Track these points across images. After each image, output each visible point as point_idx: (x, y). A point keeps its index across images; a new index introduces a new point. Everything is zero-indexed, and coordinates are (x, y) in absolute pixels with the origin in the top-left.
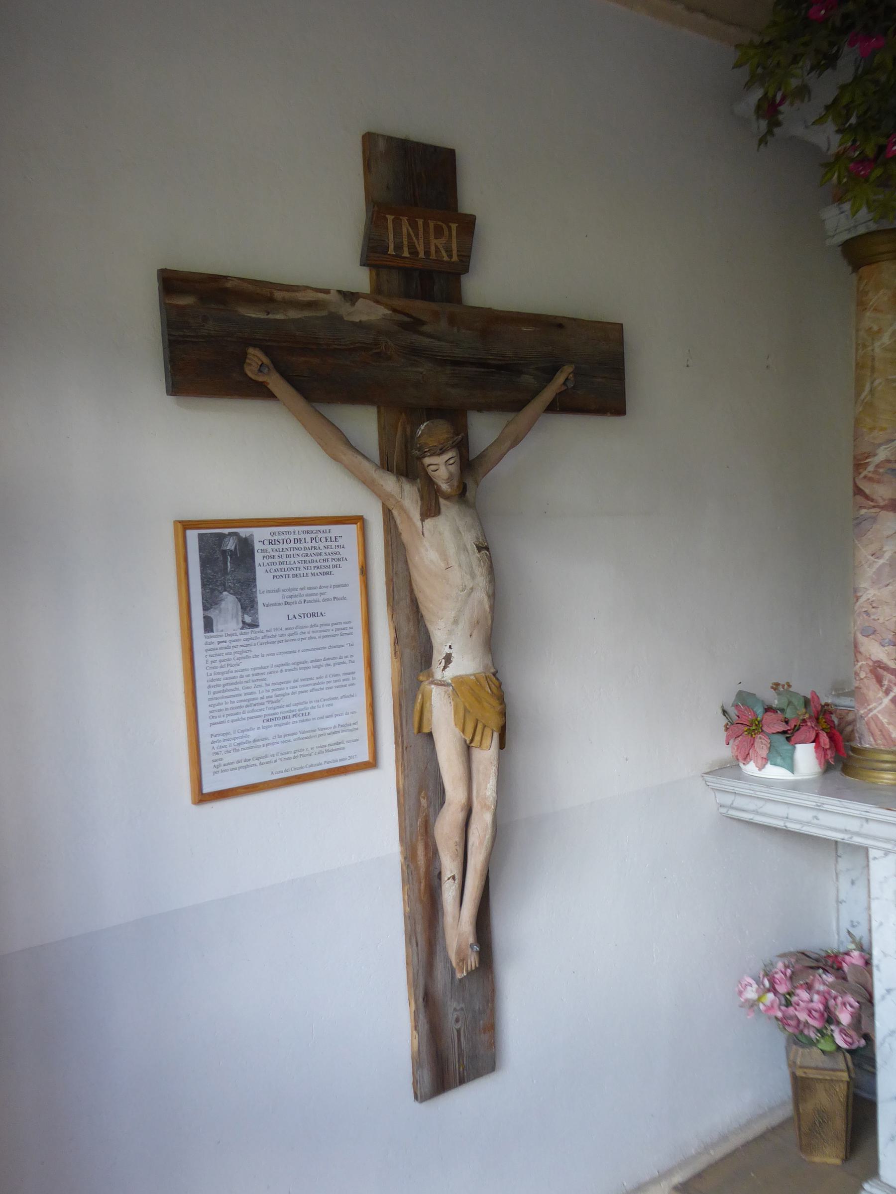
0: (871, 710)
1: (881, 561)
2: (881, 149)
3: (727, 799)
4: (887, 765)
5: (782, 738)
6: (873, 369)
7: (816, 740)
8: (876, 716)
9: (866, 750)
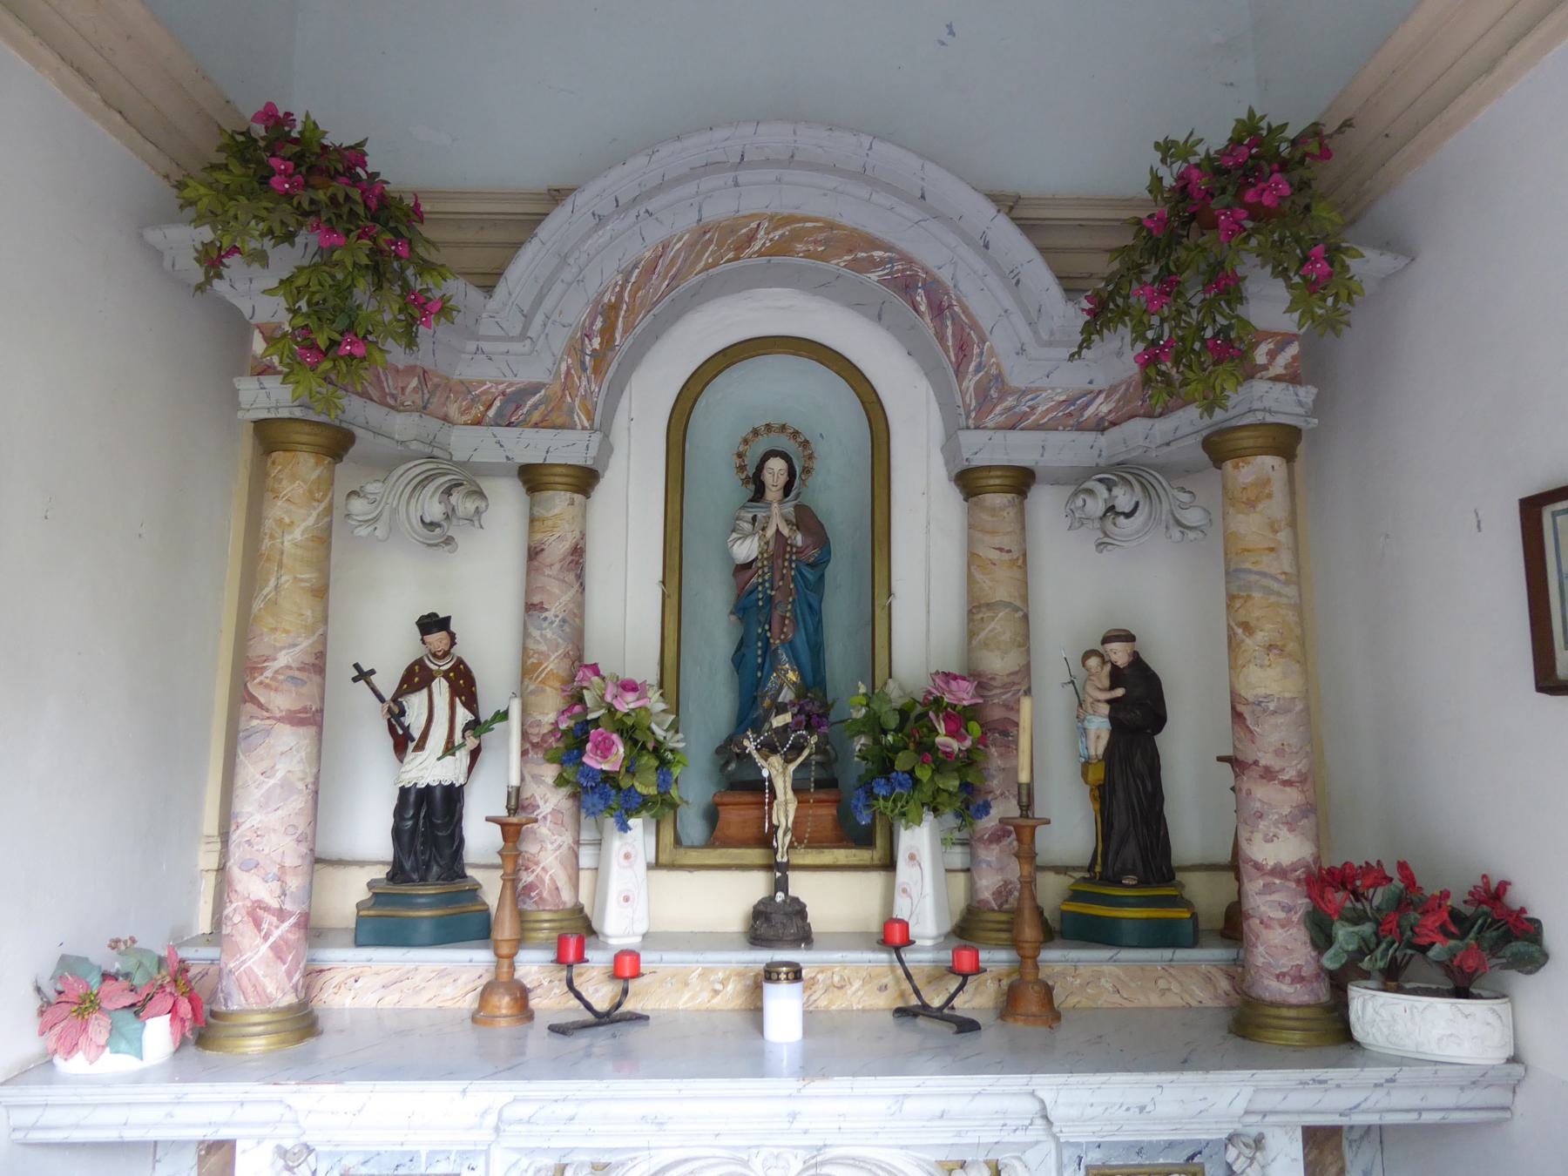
0: (244, 962)
1: (272, 782)
2: (333, 343)
3: (27, 1118)
4: (260, 1029)
5: (129, 1015)
6: (280, 565)
7: (173, 1011)
8: (250, 968)
9: (233, 1013)
